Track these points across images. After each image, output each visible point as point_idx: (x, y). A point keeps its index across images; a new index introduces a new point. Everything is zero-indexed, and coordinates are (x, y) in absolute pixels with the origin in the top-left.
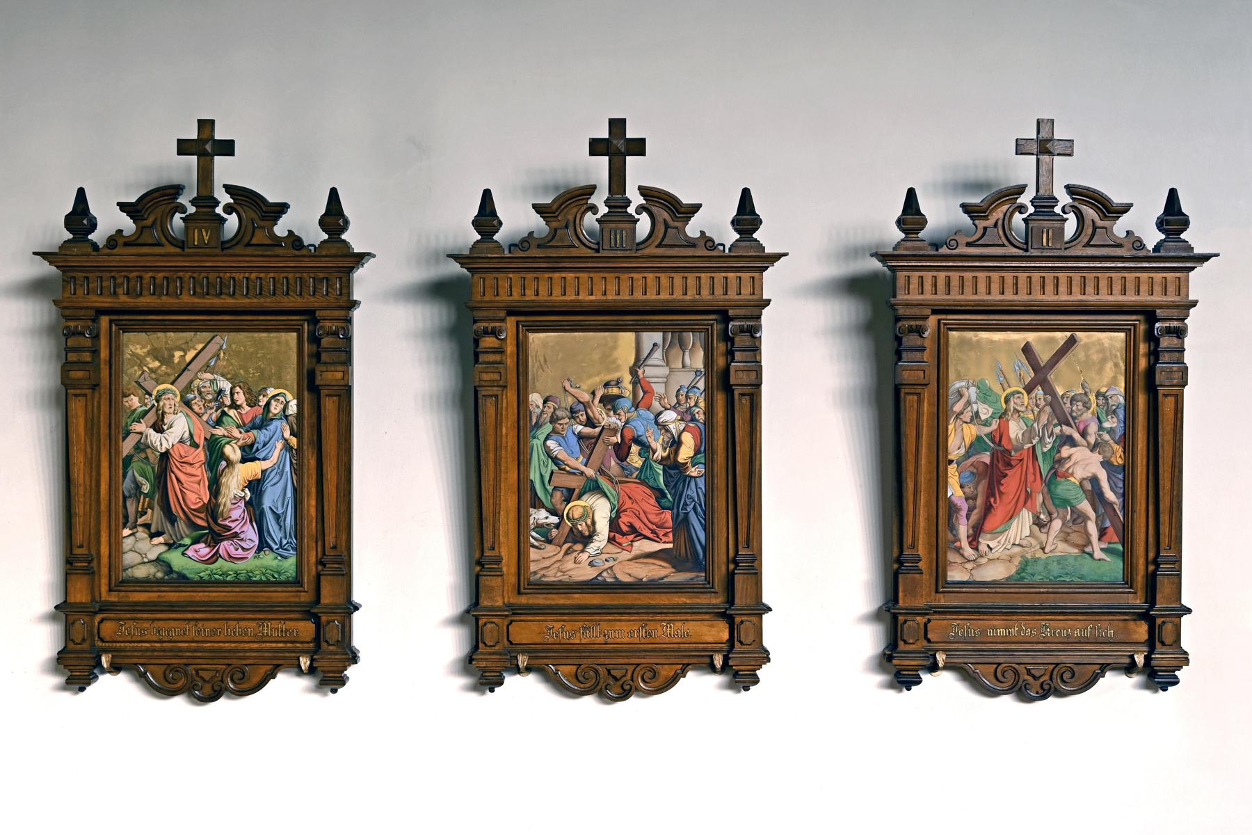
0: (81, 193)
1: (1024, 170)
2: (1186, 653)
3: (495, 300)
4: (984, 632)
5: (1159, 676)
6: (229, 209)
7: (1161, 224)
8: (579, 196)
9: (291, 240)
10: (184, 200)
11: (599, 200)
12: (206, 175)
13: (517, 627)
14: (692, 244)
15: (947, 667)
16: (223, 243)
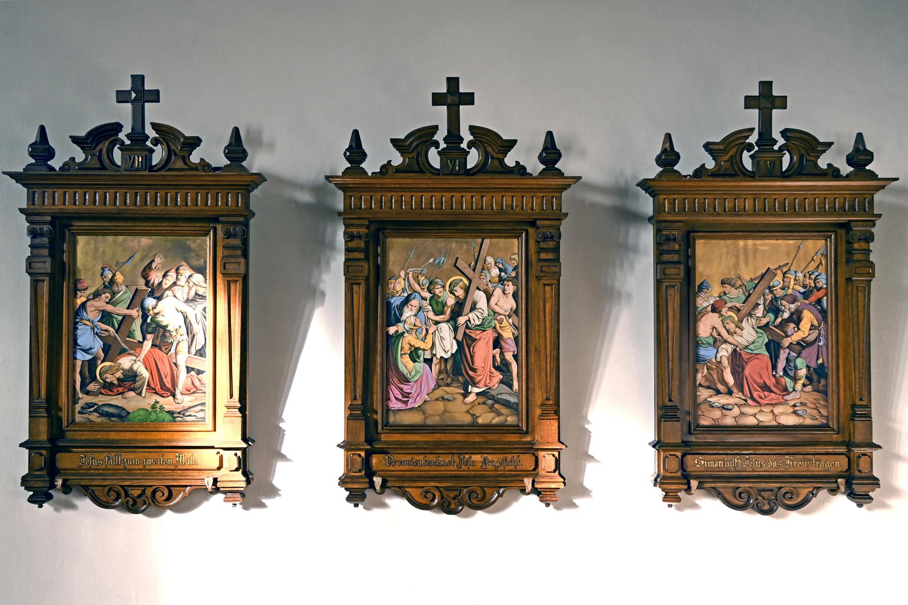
0: (356, 134)
1: (124, 114)
2: (877, 479)
3: (685, 213)
6: (156, 142)
7: (541, 159)
8: (424, 137)
9: (831, 170)
10: (122, 136)
11: (440, 136)
12: (139, 116)
13: (692, 457)
14: (195, 168)
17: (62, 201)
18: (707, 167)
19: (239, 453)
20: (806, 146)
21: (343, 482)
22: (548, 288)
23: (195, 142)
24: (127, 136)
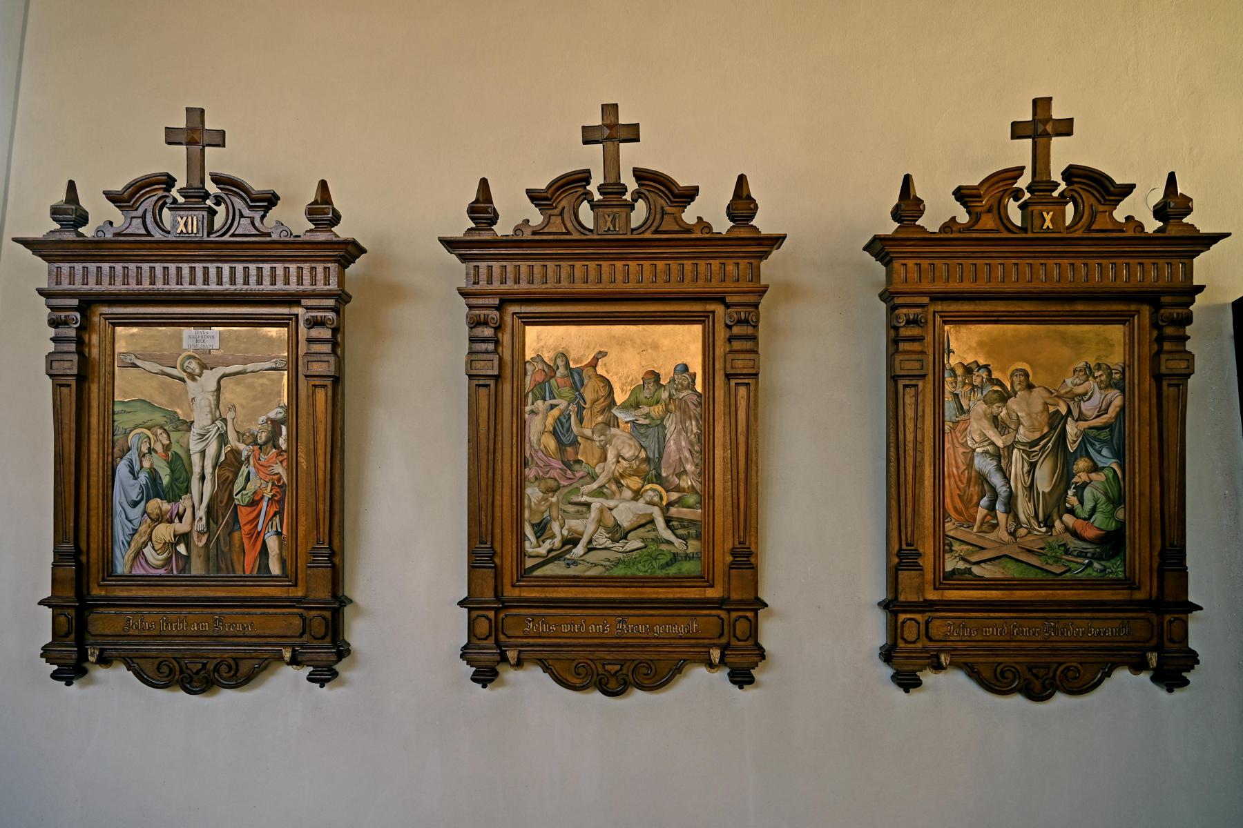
0: (484, 183)
1: (592, 158)
4: (652, 628)
5: (324, 675)
12: (612, 162)
13: (518, 616)
14: (688, 229)
15: (954, 665)
16: (633, 230)
17: (504, 276)
18: (958, 220)
19: (328, 614)
20: (1097, 187)
21: (47, 653)
22: (483, 391)
23: (690, 194)
24: (180, 191)
